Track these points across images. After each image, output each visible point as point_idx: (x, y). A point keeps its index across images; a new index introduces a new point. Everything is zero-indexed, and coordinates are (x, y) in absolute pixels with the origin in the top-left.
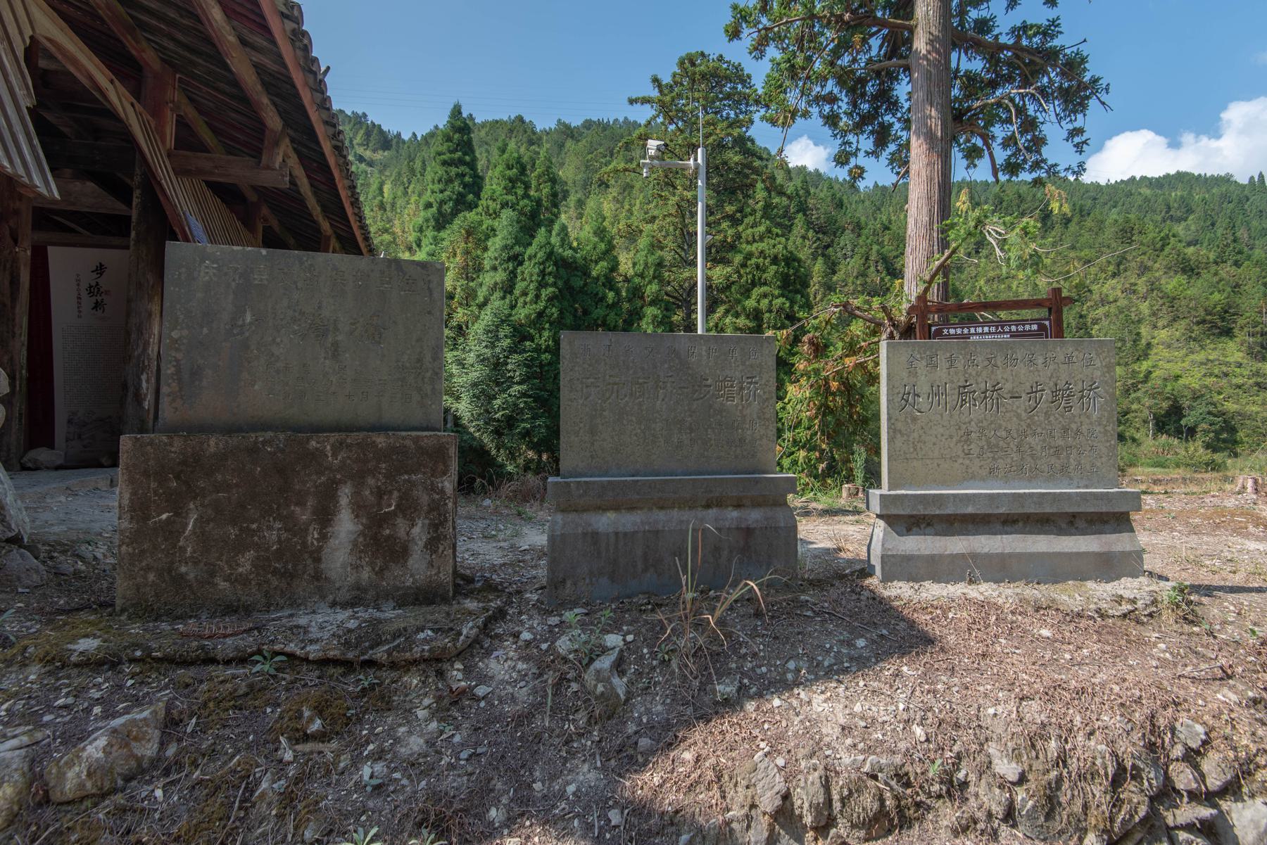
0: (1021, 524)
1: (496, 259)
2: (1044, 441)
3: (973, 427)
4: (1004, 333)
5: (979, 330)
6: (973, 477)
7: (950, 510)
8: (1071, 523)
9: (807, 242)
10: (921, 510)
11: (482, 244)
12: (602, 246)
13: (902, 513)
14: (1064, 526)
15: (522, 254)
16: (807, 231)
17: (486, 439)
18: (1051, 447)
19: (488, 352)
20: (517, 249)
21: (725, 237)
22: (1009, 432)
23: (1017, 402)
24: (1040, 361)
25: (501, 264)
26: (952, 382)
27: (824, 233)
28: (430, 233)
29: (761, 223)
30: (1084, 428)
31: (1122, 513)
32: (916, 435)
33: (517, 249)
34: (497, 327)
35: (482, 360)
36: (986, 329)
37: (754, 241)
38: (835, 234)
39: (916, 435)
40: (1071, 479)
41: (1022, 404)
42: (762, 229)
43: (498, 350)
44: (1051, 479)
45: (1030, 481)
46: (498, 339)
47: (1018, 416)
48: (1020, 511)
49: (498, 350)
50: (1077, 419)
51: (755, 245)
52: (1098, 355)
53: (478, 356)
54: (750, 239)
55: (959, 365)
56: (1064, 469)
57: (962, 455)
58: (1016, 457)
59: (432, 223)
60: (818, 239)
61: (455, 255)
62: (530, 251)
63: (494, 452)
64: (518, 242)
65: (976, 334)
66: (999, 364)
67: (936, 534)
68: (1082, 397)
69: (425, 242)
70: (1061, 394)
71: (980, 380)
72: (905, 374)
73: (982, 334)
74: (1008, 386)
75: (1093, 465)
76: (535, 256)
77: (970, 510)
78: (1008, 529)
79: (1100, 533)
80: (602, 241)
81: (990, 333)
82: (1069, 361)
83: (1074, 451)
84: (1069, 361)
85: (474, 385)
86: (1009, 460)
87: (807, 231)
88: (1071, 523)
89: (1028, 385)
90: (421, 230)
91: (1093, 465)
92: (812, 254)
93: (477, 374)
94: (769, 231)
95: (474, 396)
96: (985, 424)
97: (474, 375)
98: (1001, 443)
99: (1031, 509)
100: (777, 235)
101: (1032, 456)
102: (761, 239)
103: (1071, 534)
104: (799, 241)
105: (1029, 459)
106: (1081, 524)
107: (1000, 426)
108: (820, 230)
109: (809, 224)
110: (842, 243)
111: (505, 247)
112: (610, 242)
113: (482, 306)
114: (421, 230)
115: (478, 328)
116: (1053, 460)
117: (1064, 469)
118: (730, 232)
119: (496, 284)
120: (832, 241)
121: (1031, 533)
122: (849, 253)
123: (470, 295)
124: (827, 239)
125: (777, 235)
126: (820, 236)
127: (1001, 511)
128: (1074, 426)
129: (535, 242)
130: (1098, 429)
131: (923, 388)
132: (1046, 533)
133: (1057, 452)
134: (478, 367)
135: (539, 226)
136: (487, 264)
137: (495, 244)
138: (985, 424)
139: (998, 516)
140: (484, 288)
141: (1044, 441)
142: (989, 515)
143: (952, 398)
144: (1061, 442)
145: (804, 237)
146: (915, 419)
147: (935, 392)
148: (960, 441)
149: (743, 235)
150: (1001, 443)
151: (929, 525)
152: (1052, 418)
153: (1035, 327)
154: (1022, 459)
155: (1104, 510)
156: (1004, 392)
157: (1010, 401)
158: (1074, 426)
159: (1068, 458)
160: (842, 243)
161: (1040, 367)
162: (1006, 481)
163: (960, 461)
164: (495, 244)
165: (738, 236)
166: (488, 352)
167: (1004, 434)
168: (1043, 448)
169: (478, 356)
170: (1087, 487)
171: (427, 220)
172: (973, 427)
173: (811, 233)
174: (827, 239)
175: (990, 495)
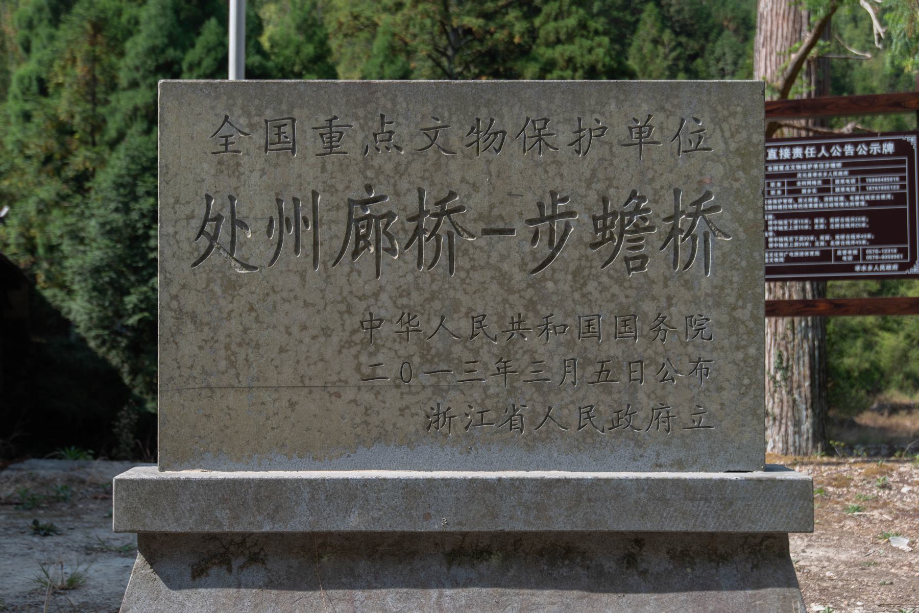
0: (495, 560)
1: (137, 69)
2: (570, 344)
3: (385, 308)
4: (831, 158)
5: (785, 153)
6: (382, 437)
7: (299, 522)
8: (630, 560)
9: (661, 50)
10: (225, 522)
11: (117, 47)
12: (309, 50)
13: (172, 527)
14: (610, 565)
15: (178, 62)
16: (661, 31)
17: (114, 358)
18: (587, 362)
19: (119, 218)
20: (171, 53)
21: (511, 36)
22: (478, 321)
23: (501, 244)
24: (563, 135)
25: (144, 78)
26: (331, 189)
27: (690, 35)
28: (43, 30)
29: (569, 14)
30: (677, 314)
31: (767, 536)
32: (234, 326)
33: (171, 53)
34: (135, 177)
35: (110, 231)
36: (798, 152)
37: (559, 41)
38: (706, 36)
39: (234, 326)
40: (639, 444)
41: (518, 247)
42: (572, 22)
43: (135, 216)
44: (587, 439)
45: (530, 448)
46: (136, 199)
47: (503, 280)
48: (487, 526)
49: (135, 216)
50: (657, 290)
51: (559, 48)
52: (718, 122)
53: (103, 225)
54: (552, 38)
55: (352, 145)
56: (621, 419)
57: (355, 379)
58: (495, 385)
59: (47, 14)
60: (680, 44)
61: (74, 60)
62: (191, 56)
63: (127, 380)
64: (172, 41)
65: (779, 161)
66: (455, 143)
67: (270, 584)
68: (673, 232)
69: (35, 44)
70: (618, 227)
71: (404, 185)
72: (207, 168)
73: (791, 160)
74: (477, 203)
75: (698, 410)
76: (199, 64)
77: (354, 522)
78: (460, 572)
79: (706, 587)
80: (310, 39)
81: (804, 159)
82: (641, 136)
83: (649, 372)
84: (641, 136)
85: (97, 271)
86: (477, 395)
87: (661, 31)
88: (630, 560)
89: (531, 199)
90: (30, 25)
91: (698, 410)
92: (669, 68)
93: (98, 254)
94: (583, 25)
95: (95, 288)
96: (416, 298)
97: (95, 255)
98: (457, 350)
99: (517, 523)
100: (597, 33)
101: (538, 383)
102: (570, 38)
103: (627, 589)
104: (648, 47)
105: (529, 391)
106: (657, 562)
107: (456, 306)
108: (683, 30)
109: (665, 20)
110: (718, 52)
111: (152, 51)
112: (323, 43)
113: (113, 145)
114: (30, 25)
115: (104, 180)
116: (593, 395)
117: (621, 419)
118: (520, 27)
119: (136, 109)
120: (703, 49)
121: (519, 584)
122: (729, 68)
123: (97, 126)
124: (693, 45)
125: (597, 33)
126: (683, 39)
127: (436, 525)
128: (649, 308)
129: (201, 42)
130: (713, 315)
131: (256, 205)
132: (558, 584)
133: (605, 373)
134: (104, 242)
135: (208, 16)
136: (123, 78)
137: (136, 46)
138: (416, 298)
139: (437, 539)
140: (119, 117)
141: (570, 344)
142: (415, 537)
143: (333, 232)
144: (613, 349)
145: (656, 42)
146: (232, 286)
147: (288, 220)
148: (350, 343)
149: (542, 33)
150: (457, 350)
151: (254, 559)
152: (591, 286)
153: (889, 148)
154: (512, 391)
155: (711, 526)
156: (464, 220)
157: (483, 242)
158: (649, 308)
159: (781, 393)
160: (718, 52)
161: (564, 152)
162: (469, 453)
163: (349, 394)
164: (136, 46)
165: (533, 33)
166: (119, 218)
167: (465, 326)
168: (568, 364)
169: (103, 225)
170: (680, 466)
171: (40, 10)
172: (385, 308)
173: (667, 36)
174: (693, 45)
175: (407, 484)
